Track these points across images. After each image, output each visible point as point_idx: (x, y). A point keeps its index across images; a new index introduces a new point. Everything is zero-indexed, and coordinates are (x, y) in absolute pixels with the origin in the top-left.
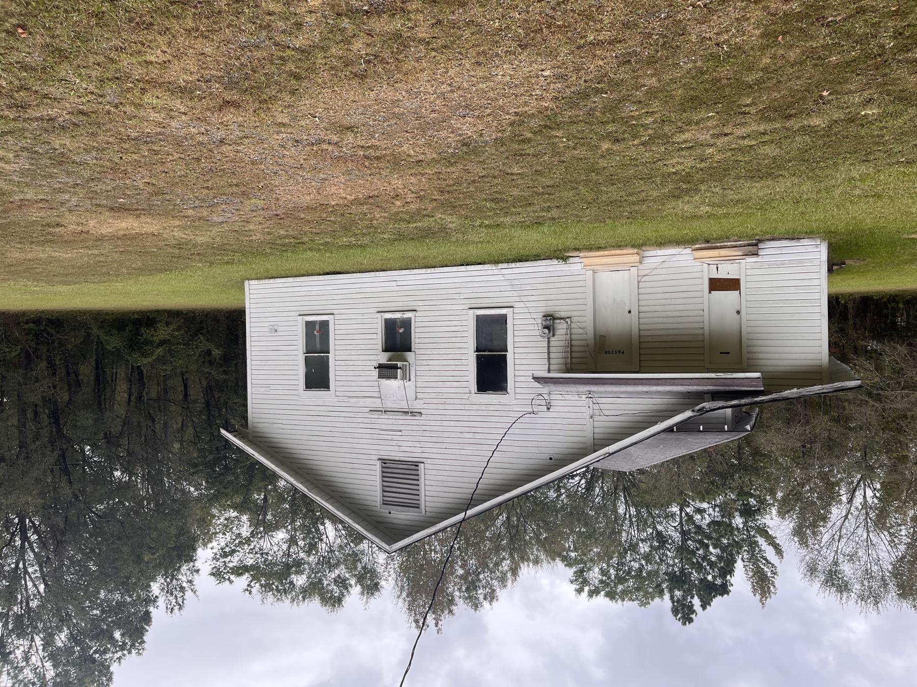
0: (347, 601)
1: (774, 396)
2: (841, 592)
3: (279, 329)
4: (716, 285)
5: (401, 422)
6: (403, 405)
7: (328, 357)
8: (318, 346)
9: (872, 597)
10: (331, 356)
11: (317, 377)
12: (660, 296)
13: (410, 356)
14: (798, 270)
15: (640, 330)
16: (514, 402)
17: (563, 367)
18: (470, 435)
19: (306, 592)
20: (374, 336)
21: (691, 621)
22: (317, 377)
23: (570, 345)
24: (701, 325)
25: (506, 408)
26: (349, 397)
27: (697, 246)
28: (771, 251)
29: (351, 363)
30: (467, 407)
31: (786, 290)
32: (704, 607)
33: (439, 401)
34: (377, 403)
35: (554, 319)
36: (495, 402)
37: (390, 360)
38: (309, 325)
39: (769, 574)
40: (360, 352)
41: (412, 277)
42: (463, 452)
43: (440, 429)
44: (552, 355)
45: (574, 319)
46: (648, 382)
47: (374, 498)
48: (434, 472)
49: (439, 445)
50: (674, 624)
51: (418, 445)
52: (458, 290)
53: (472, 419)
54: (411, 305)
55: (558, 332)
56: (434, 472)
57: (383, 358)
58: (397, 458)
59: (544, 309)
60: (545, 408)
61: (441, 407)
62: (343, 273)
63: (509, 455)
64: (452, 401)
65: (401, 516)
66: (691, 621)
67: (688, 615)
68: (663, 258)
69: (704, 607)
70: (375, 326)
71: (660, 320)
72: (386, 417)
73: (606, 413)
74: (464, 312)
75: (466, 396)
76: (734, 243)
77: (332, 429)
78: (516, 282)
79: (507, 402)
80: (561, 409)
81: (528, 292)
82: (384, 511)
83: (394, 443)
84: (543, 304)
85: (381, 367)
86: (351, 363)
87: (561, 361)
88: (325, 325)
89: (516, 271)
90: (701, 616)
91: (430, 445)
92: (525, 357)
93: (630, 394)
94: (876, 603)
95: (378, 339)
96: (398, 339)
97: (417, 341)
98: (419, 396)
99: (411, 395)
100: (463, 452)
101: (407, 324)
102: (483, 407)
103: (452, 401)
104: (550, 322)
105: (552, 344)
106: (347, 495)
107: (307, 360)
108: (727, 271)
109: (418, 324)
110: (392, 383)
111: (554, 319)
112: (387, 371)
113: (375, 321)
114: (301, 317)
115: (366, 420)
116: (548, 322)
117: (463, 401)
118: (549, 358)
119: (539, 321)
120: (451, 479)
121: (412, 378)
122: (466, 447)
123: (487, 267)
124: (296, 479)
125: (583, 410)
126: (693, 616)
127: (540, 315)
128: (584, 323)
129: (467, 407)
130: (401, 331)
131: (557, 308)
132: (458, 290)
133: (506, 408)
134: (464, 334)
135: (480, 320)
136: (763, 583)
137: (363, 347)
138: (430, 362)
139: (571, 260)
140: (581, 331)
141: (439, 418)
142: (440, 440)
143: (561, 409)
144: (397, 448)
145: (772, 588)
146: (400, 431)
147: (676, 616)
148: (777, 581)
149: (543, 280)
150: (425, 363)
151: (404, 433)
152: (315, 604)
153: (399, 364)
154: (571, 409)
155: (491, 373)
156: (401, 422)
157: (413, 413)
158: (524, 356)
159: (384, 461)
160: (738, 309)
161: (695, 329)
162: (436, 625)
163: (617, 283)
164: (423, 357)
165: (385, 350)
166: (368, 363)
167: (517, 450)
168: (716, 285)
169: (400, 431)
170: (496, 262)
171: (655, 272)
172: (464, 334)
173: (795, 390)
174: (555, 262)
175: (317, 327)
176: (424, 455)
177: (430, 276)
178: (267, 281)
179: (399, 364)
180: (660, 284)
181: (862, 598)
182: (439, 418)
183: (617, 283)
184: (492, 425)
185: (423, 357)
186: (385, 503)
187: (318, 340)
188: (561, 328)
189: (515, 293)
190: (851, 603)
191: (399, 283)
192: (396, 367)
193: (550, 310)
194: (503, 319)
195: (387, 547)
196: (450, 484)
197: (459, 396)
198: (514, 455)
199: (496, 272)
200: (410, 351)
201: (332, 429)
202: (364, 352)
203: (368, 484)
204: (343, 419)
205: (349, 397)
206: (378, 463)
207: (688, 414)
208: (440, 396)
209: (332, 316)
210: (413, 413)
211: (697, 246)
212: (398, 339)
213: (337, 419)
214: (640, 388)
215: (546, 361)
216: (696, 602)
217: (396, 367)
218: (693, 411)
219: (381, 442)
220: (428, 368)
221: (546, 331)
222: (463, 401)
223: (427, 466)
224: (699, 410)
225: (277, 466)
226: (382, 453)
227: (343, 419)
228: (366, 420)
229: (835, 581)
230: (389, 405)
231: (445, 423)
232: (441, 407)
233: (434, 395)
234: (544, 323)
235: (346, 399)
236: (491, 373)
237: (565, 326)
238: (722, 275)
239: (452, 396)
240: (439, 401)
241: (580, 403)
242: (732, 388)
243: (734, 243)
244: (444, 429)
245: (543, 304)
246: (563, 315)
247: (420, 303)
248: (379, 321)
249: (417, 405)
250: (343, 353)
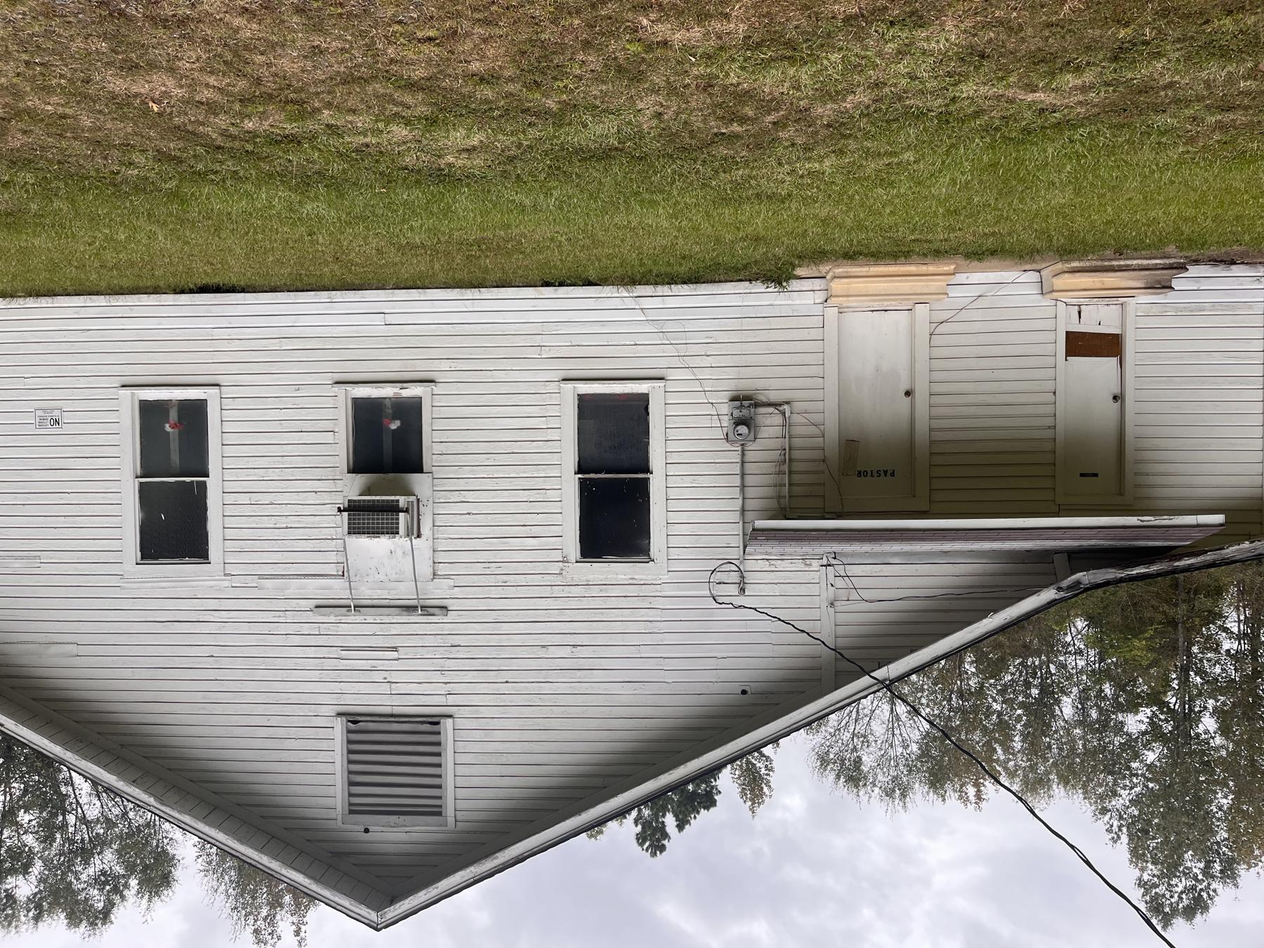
0: (118, 914)
1: (1209, 557)
2: (857, 786)
3: (67, 418)
4: (1080, 344)
5: (396, 629)
6: (405, 592)
7: (203, 487)
8: (175, 458)
9: (897, 790)
10: (213, 485)
11: (174, 527)
12: (973, 363)
13: (418, 482)
14: (1227, 321)
15: (931, 430)
16: (666, 578)
17: (773, 504)
18: (566, 652)
19: (39, 908)
20: (329, 438)
21: (662, 849)
22: (174, 527)
23: (787, 460)
24: (1049, 422)
25: (646, 591)
26: (261, 576)
27: (1075, 264)
28: (1201, 286)
29: (266, 499)
30: (557, 591)
31: (1205, 359)
32: (680, 827)
33: (491, 580)
34: (337, 589)
35: (757, 405)
36: (622, 578)
37: (368, 491)
38: (151, 413)
39: (763, 771)
40: (288, 474)
41: (427, 307)
42: (546, 688)
43: (494, 640)
44: (749, 480)
45: (798, 406)
46: (995, 533)
47: (330, 802)
48: (478, 735)
49: (491, 676)
50: (640, 854)
51: (437, 677)
52: (538, 340)
53: (568, 615)
54: (422, 368)
55: (765, 432)
56: (478, 735)
57: (353, 487)
58: (388, 710)
59: (731, 385)
60: (734, 590)
61: (495, 592)
62: (243, 291)
63: (648, 689)
64: (521, 580)
65: (394, 835)
66: (662, 849)
67: (658, 840)
68: (976, 291)
69: (680, 827)
70: (330, 414)
71: (972, 410)
72: (359, 619)
73: (866, 594)
74: (552, 387)
75: (555, 568)
76: (1145, 262)
77: (216, 651)
78: (669, 327)
79: (649, 578)
80: (766, 590)
81: (694, 348)
82: (353, 828)
83: (378, 677)
84: (731, 373)
85: (353, 508)
86: (266, 499)
87: (769, 491)
88: (194, 414)
89: (671, 302)
90: (677, 840)
91: (469, 677)
92: (690, 485)
93: (911, 558)
94: (904, 796)
95: (338, 442)
96: (387, 447)
97: (437, 448)
98: (442, 569)
99: (425, 569)
100: (546, 688)
101: (410, 412)
102: (595, 591)
103: (521, 580)
104: (746, 409)
105: (750, 456)
106: (14, 671)
107: (144, 491)
108: (1100, 319)
109: (438, 413)
110: (382, 543)
111: (757, 405)
112: (369, 517)
113: (329, 402)
114: (127, 392)
115: (306, 629)
116: (745, 412)
117: (548, 580)
118: (743, 487)
119: (725, 409)
120: (517, 747)
121: (426, 530)
122: (553, 676)
123: (607, 291)
124: (120, 775)
125: (814, 589)
126: (665, 842)
127: (724, 398)
128: (820, 410)
129: (557, 591)
130: (394, 425)
131: (760, 384)
132: (538, 340)
133: (646, 591)
134: (553, 435)
135: (585, 404)
136: (754, 786)
137: (299, 462)
138: (470, 496)
139: (795, 285)
140: (813, 430)
141: (491, 616)
142: (495, 664)
143: (766, 590)
144: (385, 688)
145: (765, 789)
146: (395, 649)
147: (641, 845)
148: (774, 779)
149: (734, 324)
150: (455, 497)
151: (402, 653)
152: (56, 925)
153: (403, 501)
154: (789, 589)
155: (614, 515)
156: (396, 629)
157: (426, 610)
158: (687, 482)
159: (352, 718)
160: (1117, 391)
161: (1038, 428)
162: (297, 933)
163: (886, 334)
164: (450, 485)
165: (355, 469)
166: (326, 498)
167: (670, 677)
168: (1080, 344)
169: (395, 649)
170: (630, 280)
171: (964, 315)
172: (553, 435)
173: (1246, 545)
174: (759, 287)
175: (173, 415)
176: (451, 700)
177: (469, 306)
178: (30, 302)
179: (403, 501)
180: (972, 340)
181: (889, 793)
182: (491, 616)
183: (886, 334)
184: (617, 627)
185: (450, 485)
186: (353, 810)
187: (174, 446)
188: (770, 423)
189: (670, 350)
190: (875, 800)
191: (390, 319)
192: (394, 509)
193: (746, 386)
194: (640, 405)
195: (373, 916)
196: (513, 759)
197: (540, 568)
198: (664, 689)
199: (630, 303)
200: (420, 470)
201: (216, 651)
202: (299, 474)
203: (316, 771)
204: (245, 628)
205: (261, 576)
206: (339, 725)
207: (1049, 595)
208: (493, 569)
209: (215, 390)
210: (426, 610)
211: (1075, 264)
212: (387, 447)
213: (228, 628)
214: (896, 547)
215: (736, 492)
216: (670, 821)
217: (394, 509)
218: (1059, 589)
219: (345, 676)
220: (464, 508)
221: (743, 429)
222: (548, 580)
223: (461, 723)
224: (1069, 588)
225: (64, 745)
226: (349, 699)
227: (245, 628)
228: (306, 629)
229: (853, 775)
230: (366, 592)
231: (506, 628)
232: (495, 592)
233: (478, 569)
234: (736, 413)
235: (252, 582)
236: (614, 515)
237: (778, 419)
238: (1088, 326)
239: (522, 568)
240: (491, 580)
241: (814, 577)
242: (1151, 544)
243: (1145, 262)
244: (504, 640)
245: (731, 373)
246: (774, 396)
247: (445, 365)
248: (342, 397)
249: (437, 591)
250: (242, 475)
